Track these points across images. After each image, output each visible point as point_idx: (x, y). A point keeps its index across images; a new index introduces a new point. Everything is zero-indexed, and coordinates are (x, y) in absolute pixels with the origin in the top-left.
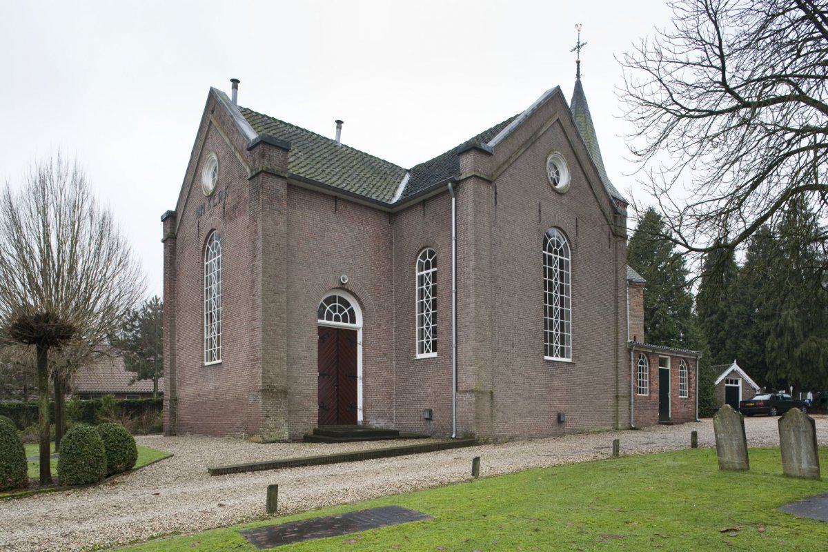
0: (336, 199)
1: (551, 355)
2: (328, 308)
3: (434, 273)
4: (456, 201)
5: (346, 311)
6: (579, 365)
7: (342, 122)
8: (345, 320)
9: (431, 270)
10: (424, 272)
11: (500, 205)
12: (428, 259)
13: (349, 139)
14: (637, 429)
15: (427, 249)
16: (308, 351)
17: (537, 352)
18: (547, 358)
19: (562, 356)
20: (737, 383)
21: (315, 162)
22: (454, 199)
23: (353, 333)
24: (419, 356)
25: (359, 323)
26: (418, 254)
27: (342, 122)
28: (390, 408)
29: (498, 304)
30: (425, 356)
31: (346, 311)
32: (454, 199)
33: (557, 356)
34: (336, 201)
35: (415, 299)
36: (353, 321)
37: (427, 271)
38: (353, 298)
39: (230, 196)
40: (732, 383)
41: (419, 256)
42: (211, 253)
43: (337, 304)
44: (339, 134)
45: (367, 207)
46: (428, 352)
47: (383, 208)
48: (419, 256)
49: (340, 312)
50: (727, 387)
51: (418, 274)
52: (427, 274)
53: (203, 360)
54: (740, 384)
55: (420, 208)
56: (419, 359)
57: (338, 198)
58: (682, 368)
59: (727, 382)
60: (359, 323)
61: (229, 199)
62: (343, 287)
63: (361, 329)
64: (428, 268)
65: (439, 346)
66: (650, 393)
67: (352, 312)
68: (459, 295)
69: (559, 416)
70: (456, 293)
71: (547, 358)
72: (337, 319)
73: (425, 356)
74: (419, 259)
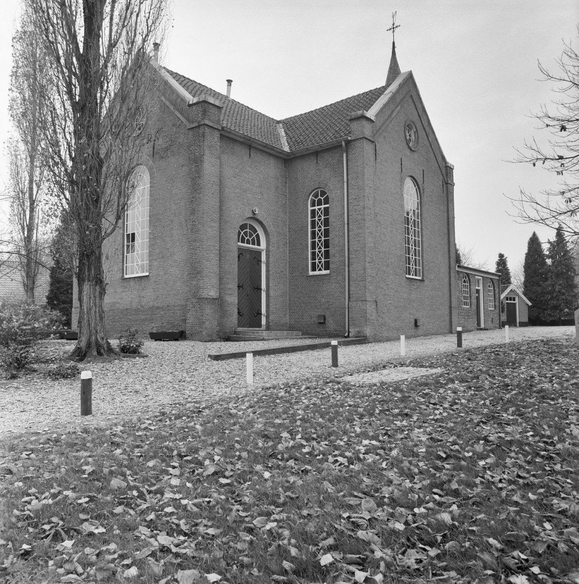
0: (250, 147)
1: (410, 274)
2: (242, 233)
3: (326, 209)
4: (347, 156)
5: (254, 235)
6: (426, 282)
7: (232, 81)
8: (253, 244)
9: (323, 206)
10: (316, 208)
11: (378, 160)
12: (319, 197)
13: (237, 95)
14: (487, 330)
15: (319, 190)
16: (233, 267)
17: (401, 272)
18: (407, 276)
19: (416, 275)
20: (514, 299)
21: (230, 116)
22: (345, 155)
23: (259, 253)
24: (311, 273)
25: (263, 245)
26: (311, 193)
27: (232, 81)
28: (285, 315)
29: (378, 234)
30: (317, 273)
31: (254, 235)
32: (345, 155)
33: (413, 275)
34: (250, 149)
35: (308, 228)
36: (259, 244)
37: (319, 207)
38: (256, 222)
39: (160, 140)
40: (510, 300)
41: (312, 194)
42: (419, 228)
43: (248, 230)
44: (229, 91)
45: (270, 154)
46: (320, 270)
47: (281, 155)
48: (312, 194)
49: (250, 237)
50: (507, 303)
51: (310, 208)
52: (319, 209)
53: (123, 273)
54: (517, 301)
55: (313, 158)
56: (311, 276)
57: (250, 145)
58: (489, 287)
59: (507, 300)
60: (263, 245)
61: (160, 142)
62: (254, 218)
63: (265, 251)
64: (320, 203)
65: (331, 266)
66: (471, 305)
67: (258, 236)
68: (351, 227)
69: (416, 321)
70: (348, 224)
71: (407, 276)
72: (248, 242)
73: (317, 273)
74: (311, 197)
